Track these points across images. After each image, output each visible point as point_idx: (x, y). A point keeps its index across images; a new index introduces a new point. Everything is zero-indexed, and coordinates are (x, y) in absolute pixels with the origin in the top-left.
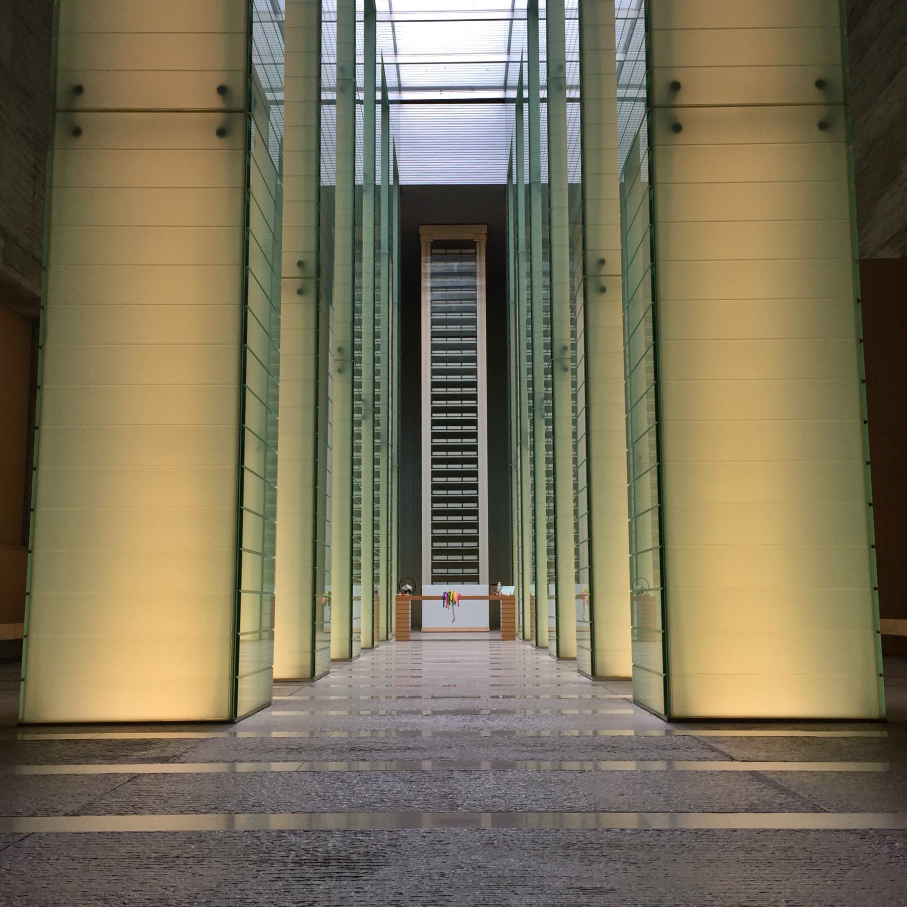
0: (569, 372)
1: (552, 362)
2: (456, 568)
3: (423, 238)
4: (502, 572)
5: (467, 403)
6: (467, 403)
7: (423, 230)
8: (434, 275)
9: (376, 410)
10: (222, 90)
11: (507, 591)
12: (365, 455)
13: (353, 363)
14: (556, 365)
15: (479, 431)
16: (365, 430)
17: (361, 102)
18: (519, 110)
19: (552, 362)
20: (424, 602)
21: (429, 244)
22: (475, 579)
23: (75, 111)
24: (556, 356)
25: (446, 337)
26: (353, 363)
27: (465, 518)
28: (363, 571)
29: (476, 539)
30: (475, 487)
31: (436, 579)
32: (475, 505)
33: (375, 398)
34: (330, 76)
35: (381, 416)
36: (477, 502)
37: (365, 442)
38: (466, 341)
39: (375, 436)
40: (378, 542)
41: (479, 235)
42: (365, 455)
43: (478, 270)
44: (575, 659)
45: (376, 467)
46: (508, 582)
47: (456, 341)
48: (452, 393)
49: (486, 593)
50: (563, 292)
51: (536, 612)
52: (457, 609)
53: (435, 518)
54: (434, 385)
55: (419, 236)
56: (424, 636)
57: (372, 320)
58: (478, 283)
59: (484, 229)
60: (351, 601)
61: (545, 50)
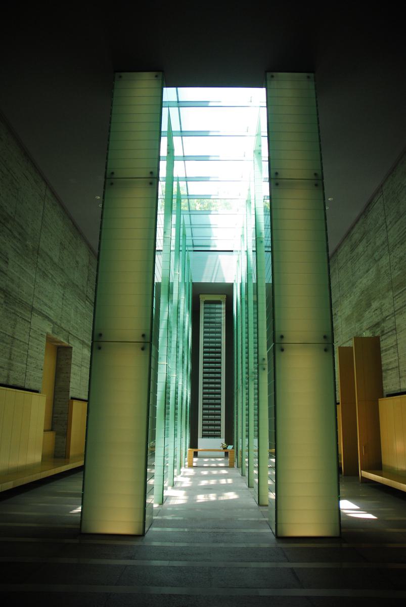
2: (212, 433)
3: (201, 299)
6: (217, 391)
7: (201, 296)
10: (316, 174)
14: (260, 367)
15: (222, 336)
17: (181, 251)
18: (171, 107)
22: (219, 436)
23: (315, 180)
24: (260, 362)
27: (216, 396)
28: (178, 416)
29: (220, 394)
30: (220, 388)
31: (204, 436)
34: (181, 235)
41: (222, 298)
44: (267, 506)
53: (204, 406)
55: (199, 299)
59: (225, 296)
61: (160, 201)
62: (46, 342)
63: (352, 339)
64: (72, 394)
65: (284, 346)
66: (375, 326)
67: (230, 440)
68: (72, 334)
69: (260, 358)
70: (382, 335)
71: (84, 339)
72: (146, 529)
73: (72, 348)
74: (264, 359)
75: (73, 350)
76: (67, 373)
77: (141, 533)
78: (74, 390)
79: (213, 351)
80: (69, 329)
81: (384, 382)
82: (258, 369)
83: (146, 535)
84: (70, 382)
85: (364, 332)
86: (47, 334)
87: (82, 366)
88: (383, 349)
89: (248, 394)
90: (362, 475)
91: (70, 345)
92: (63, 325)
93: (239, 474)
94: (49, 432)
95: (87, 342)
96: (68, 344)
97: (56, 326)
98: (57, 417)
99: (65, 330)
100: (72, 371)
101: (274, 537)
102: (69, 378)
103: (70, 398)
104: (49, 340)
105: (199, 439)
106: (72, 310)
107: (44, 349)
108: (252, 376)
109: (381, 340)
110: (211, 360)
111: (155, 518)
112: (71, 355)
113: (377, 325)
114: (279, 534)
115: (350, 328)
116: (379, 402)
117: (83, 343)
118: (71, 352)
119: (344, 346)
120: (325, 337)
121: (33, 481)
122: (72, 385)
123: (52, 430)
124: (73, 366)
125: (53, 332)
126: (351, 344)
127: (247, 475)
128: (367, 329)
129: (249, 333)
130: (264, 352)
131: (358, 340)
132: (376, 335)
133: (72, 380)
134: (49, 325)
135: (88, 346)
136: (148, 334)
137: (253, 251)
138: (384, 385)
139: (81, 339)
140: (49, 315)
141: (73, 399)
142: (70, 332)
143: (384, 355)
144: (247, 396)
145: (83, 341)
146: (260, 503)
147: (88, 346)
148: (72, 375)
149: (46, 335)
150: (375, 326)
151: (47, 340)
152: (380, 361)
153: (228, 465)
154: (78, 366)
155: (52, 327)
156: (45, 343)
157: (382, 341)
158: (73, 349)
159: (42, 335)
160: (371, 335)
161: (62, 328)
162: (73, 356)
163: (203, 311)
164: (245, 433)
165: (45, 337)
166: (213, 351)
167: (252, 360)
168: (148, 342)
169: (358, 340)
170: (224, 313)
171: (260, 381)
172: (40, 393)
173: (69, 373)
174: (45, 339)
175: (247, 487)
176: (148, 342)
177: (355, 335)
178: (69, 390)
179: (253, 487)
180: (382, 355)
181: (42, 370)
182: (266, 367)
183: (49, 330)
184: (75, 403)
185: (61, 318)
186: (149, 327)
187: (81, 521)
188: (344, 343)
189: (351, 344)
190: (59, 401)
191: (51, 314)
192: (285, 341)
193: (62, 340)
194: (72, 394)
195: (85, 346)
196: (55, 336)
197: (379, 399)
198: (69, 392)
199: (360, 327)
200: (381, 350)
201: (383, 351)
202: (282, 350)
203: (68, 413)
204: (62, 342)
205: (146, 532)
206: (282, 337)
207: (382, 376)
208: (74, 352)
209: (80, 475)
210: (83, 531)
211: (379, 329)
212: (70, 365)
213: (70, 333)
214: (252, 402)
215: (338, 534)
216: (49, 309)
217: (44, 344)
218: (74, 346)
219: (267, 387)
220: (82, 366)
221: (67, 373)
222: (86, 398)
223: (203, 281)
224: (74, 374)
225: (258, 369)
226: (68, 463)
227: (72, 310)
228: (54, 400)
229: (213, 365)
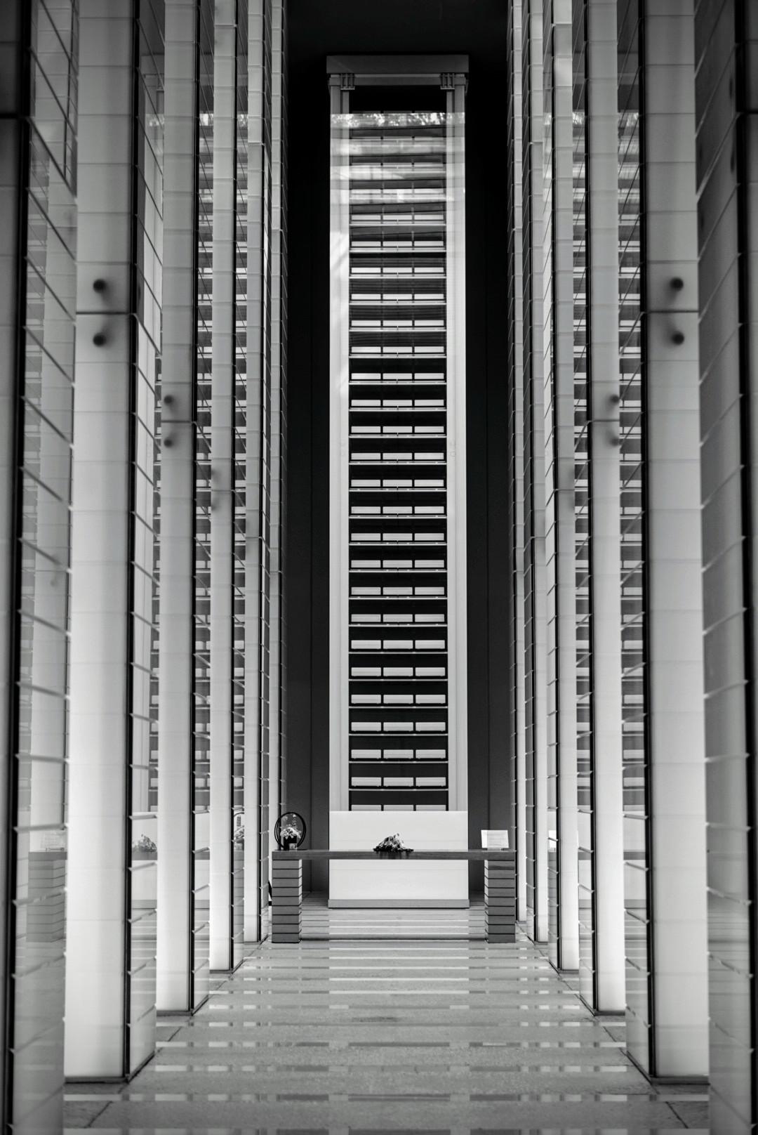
0: (619, 447)
1: (590, 427)
3: (334, 80)
4: (490, 802)
5: (424, 378)
7: (334, 66)
8: (354, 134)
9: (237, 499)
11: (494, 840)
12: (218, 567)
13: (194, 428)
16: (219, 521)
19: (590, 427)
20: (333, 863)
21: (346, 97)
22: (439, 798)
24: (597, 414)
25: (381, 240)
26: (194, 428)
31: (358, 798)
32: (440, 536)
33: (237, 472)
35: (248, 484)
36: (444, 558)
37: (217, 539)
38: (424, 405)
39: (237, 525)
40: (242, 665)
42: (218, 567)
43: (449, 229)
45: (238, 456)
46: (506, 821)
47: (393, 378)
48: (399, 384)
49: (461, 843)
50: (611, 325)
51: (558, 868)
52: (400, 863)
54: (357, 339)
56: (337, 923)
57: (229, 309)
58: (449, 173)
60: (192, 858)
67: (490, 802)
69: (658, 277)
74: (677, 284)
82: (644, 341)
89: (588, 552)
105: (333, 814)
110: (393, 378)
129: (597, 261)
137: (628, 856)
144: (585, 671)
153: (482, 931)
163: (346, 225)
164: (572, 781)
167: (611, 299)
168: (118, 313)
171: (655, 404)
175: (589, 1014)
176: (118, 313)
182: (690, 325)
186: (123, 255)
219: (701, 708)
223: (332, 168)
225: (644, 341)
229: (402, 378)
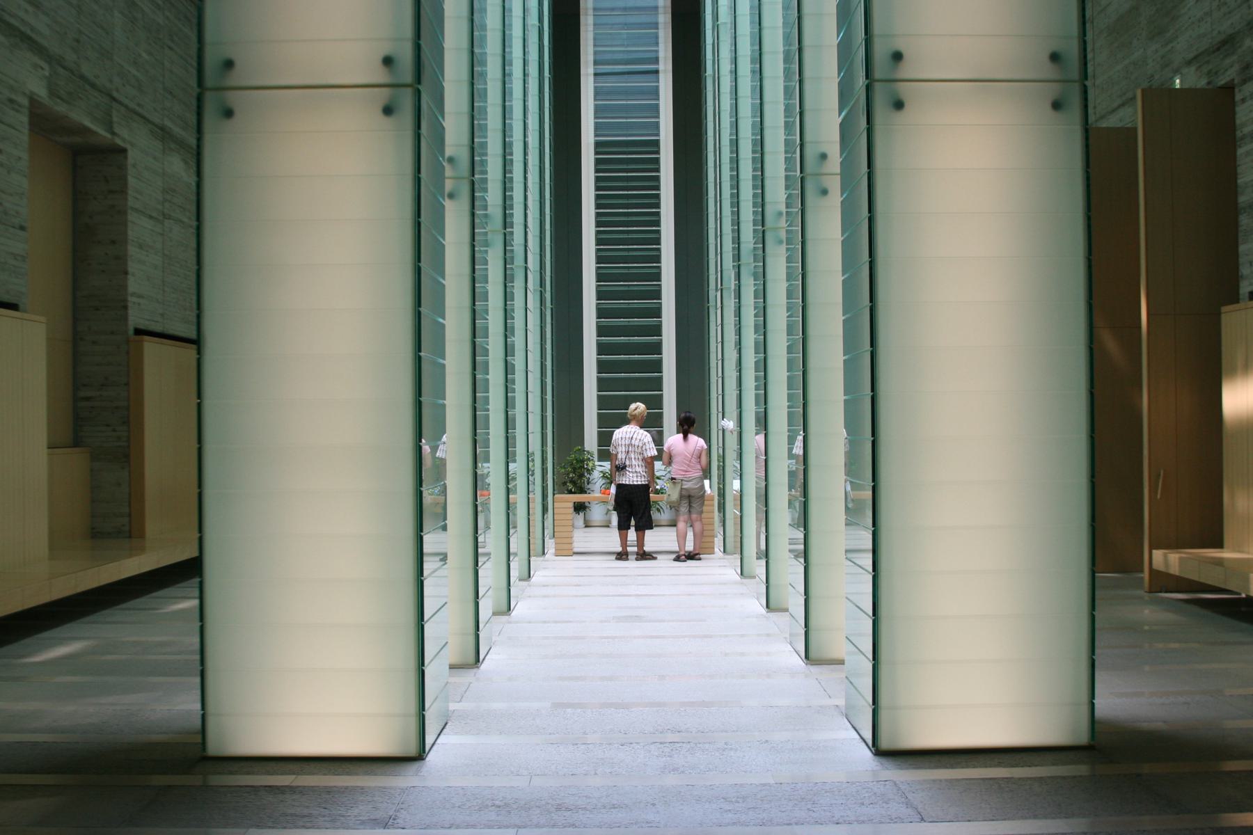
62: (31, 130)
63: (1134, 98)
64: (137, 317)
65: (904, 90)
66: (1218, 49)
68: (121, 103)
70: (1244, 82)
71: (168, 123)
72: (429, 740)
73: (124, 151)
75: (130, 161)
76: (113, 242)
77: (412, 750)
78: (141, 301)
79: (628, 164)
80: (111, 81)
81: (1242, 248)
83: (431, 758)
84: (126, 273)
85: (1177, 71)
86: (34, 101)
87: (166, 216)
88: (1246, 130)
90: (1155, 566)
91: (119, 142)
92: (86, 69)
93: (732, 574)
94: (69, 450)
95: (177, 130)
96: (109, 136)
97: (61, 70)
98: (88, 399)
99: (93, 86)
100: (131, 234)
101: (867, 754)
102: (121, 259)
103: (131, 332)
104: (44, 124)
106: (116, 14)
107: (25, 156)
108: (779, 226)
109: (1238, 97)
111: (452, 706)
112: (124, 179)
113: (1227, 44)
114: (885, 744)
115: (1127, 62)
116: (1223, 317)
117: (163, 134)
118: (122, 167)
119: (1104, 125)
120: (1055, 57)
121: (26, 607)
122: (133, 285)
123: (76, 443)
124: (132, 217)
125: (53, 93)
126: (1132, 116)
127: (761, 571)
128: (1189, 63)
130: (826, 126)
131: (1159, 99)
132: (1222, 81)
133: (132, 267)
134: (36, 66)
135: (181, 144)
136: (405, 55)
138: (1241, 260)
139: (157, 121)
140: (32, 29)
141: (139, 332)
142: (115, 94)
143: (1248, 153)
145: (162, 129)
146: (812, 655)
147: (181, 144)
148: (132, 250)
149: (25, 102)
150: (1218, 49)
151: (31, 124)
152: (1234, 176)
154: (151, 217)
155: (47, 74)
156: (26, 131)
157: (1243, 100)
158: (130, 153)
159: (11, 101)
160: (1202, 83)
161: (82, 77)
162: (131, 181)
165: (26, 111)
166: (628, 164)
169: (1159, 99)
170: (665, 71)
172: (25, 311)
173: (119, 241)
174: (25, 119)
177: (1145, 85)
178: (126, 300)
179: (786, 610)
180: (1240, 151)
181: (22, 228)
182: (834, 184)
183: (41, 92)
184: (151, 348)
185: (78, 41)
186: (408, 31)
187: (204, 717)
188: (1102, 117)
189: (1132, 116)
190: (94, 343)
191: (39, 25)
192: (906, 70)
193: (87, 123)
194: (137, 317)
195: (173, 146)
196: (61, 108)
197: (1224, 309)
198: (126, 308)
199: (1163, 57)
200: (1239, 134)
201: (1243, 138)
202: (899, 105)
203: (127, 384)
204: (86, 131)
205: (427, 749)
206: (898, 57)
207: (1236, 224)
208: (134, 166)
209: (191, 586)
210: (213, 749)
211: (1235, 57)
212: (123, 213)
213: (114, 99)
214: (779, 319)
215: (1083, 738)
216: (30, 9)
217: (24, 136)
218: (132, 145)
220: (166, 216)
221: (113, 242)
222: (193, 336)
224: (141, 247)
226: (141, 550)
227: (116, 14)
228: (77, 338)
